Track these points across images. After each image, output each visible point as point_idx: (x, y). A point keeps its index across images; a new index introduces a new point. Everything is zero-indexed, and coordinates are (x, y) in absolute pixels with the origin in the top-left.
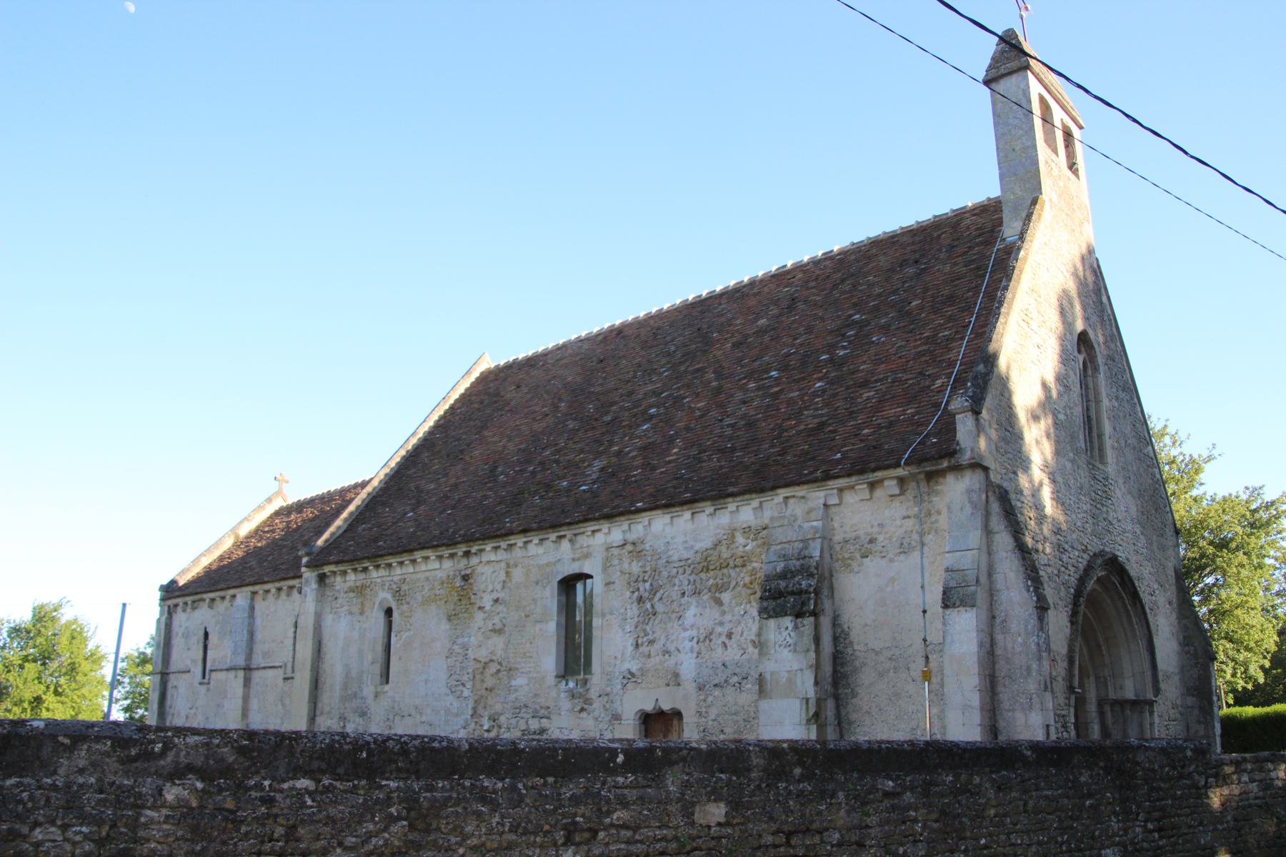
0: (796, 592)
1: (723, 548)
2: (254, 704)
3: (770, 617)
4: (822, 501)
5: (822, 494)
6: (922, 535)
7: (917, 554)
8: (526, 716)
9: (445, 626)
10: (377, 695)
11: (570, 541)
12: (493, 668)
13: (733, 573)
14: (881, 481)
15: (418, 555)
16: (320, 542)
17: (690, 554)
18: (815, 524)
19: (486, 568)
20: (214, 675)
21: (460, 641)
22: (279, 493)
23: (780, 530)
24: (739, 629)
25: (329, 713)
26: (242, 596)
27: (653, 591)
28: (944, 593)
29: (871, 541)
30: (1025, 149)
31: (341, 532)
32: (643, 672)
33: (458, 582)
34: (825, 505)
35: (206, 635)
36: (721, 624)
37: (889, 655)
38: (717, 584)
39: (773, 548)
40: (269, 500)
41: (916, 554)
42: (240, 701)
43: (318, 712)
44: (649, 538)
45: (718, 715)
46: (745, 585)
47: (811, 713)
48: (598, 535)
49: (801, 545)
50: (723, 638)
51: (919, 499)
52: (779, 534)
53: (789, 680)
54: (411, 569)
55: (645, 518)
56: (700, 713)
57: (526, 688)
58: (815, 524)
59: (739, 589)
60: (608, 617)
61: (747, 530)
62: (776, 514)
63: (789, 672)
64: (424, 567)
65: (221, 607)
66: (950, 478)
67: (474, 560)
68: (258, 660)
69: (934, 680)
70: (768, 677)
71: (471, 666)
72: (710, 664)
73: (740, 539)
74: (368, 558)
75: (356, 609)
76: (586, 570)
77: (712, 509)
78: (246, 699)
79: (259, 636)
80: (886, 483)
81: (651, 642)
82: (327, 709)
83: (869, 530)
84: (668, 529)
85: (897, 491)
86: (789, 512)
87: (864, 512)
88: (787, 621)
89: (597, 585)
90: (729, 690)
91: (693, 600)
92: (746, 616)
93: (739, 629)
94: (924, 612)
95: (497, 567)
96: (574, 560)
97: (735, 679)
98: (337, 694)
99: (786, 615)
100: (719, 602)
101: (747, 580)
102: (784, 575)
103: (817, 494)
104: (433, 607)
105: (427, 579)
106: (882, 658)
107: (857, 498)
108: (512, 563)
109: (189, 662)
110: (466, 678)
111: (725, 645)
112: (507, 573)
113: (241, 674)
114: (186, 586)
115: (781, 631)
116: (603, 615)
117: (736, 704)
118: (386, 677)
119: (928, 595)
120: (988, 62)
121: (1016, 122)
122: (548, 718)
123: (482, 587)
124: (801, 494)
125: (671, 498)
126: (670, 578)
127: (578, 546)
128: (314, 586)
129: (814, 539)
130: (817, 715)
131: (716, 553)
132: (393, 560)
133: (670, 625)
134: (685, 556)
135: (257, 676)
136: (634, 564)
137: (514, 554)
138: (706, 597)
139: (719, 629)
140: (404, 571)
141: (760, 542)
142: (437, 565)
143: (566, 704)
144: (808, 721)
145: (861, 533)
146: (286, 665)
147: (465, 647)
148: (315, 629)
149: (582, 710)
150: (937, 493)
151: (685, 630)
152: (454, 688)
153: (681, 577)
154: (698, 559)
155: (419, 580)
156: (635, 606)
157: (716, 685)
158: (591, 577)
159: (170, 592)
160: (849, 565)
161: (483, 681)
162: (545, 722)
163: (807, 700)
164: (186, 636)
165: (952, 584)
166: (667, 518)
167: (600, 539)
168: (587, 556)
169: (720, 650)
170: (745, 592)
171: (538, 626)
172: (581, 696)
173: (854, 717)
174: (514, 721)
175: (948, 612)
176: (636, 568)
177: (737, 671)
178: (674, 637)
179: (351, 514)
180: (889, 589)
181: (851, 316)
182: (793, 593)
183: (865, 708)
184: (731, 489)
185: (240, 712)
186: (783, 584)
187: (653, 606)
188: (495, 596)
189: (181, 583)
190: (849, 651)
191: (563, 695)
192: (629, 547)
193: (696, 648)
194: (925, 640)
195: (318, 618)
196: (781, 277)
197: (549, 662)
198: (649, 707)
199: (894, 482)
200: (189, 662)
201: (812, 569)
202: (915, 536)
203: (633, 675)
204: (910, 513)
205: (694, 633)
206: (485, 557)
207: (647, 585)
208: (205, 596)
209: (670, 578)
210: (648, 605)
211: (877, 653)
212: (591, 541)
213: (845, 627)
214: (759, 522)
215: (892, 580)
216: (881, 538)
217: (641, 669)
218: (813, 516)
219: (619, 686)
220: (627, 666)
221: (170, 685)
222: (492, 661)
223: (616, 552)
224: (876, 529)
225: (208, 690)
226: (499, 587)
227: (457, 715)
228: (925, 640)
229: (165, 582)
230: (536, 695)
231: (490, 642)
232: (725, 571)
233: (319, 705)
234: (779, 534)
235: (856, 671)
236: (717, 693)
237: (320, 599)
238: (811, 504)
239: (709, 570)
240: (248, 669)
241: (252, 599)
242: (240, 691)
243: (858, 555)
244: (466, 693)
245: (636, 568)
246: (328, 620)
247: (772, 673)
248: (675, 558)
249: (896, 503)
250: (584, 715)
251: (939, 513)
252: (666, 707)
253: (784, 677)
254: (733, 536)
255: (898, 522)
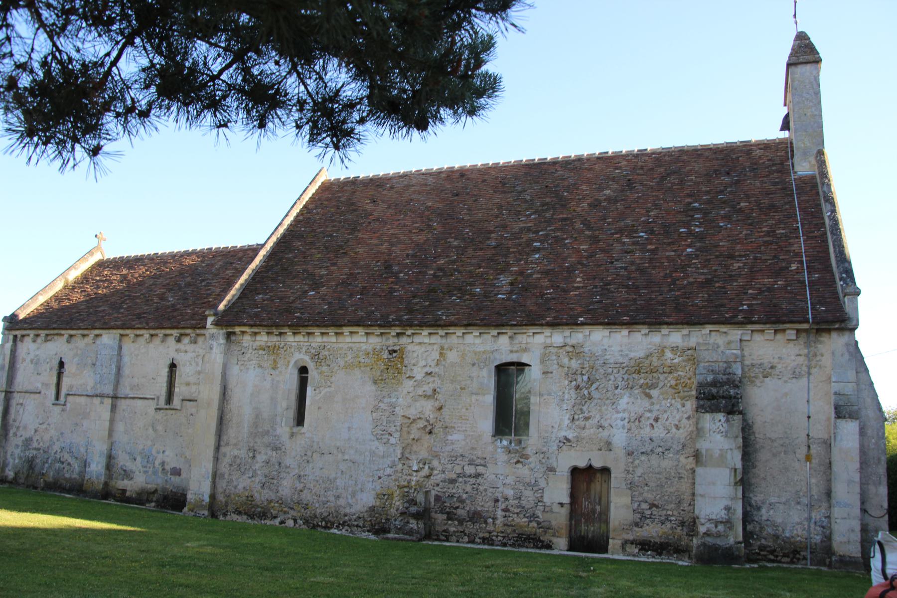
0: (721, 396)
1: (655, 359)
2: (120, 427)
3: (707, 412)
4: (739, 337)
5: (740, 332)
6: (809, 367)
7: (805, 379)
8: (462, 463)
9: (370, 388)
10: (292, 435)
11: (511, 338)
12: (421, 424)
13: (662, 377)
14: (784, 330)
15: (346, 330)
16: (221, 307)
17: (626, 360)
18: (735, 351)
19: (417, 348)
20: (70, 398)
21: (386, 400)
22: (98, 248)
23: (706, 352)
24: (665, 416)
25: (235, 445)
26: (108, 338)
27: (591, 381)
28: (836, 408)
29: (772, 368)
30: (814, 116)
31: (236, 297)
32: (578, 439)
33: (385, 355)
34: (741, 340)
35: (61, 364)
36: (650, 411)
37: (781, 442)
38: (647, 383)
39: (702, 365)
40: (91, 253)
41: (804, 380)
42: (107, 424)
43: (222, 443)
44: (587, 344)
45: (644, 474)
46: (671, 386)
47: (739, 478)
48: (537, 336)
49: (725, 365)
50: (651, 421)
51: (808, 345)
52: (706, 355)
53: (721, 456)
54: (334, 339)
55: (586, 330)
56: (628, 472)
57: (463, 443)
58: (735, 351)
59: (665, 388)
60: (545, 397)
61: (674, 349)
62: (701, 341)
63: (720, 450)
64: (348, 339)
65: (80, 343)
66: (834, 335)
67: (404, 340)
68: (124, 390)
69: (813, 461)
70: (704, 452)
71: (399, 421)
72: (639, 439)
73: (669, 354)
74: (289, 326)
75: (267, 364)
76: (524, 360)
77: (647, 331)
78: (112, 421)
79: (126, 371)
80: (788, 332)
81: (587, 419)
82: (233, 441)
83: (772, 361)
84: (606, 341)
85: (794, 338)
86: (712, 341)
87: (767, 348)
88: (721, 416)
89: (534, 373)
90: (654, 457)
91: (627, 392)
92: (672, 408)
93: (665, 416)
94: (809, 417)
95: (429, 348)
96: (512, 352)
97: (660, 449)
98: (246, 430)
99: (720, 412)
100: (649, 396)
101: (673, 383)
102: (714, 383)
103: (736, 332)
104: (357, 371)
105: (350, 348)
106: (776, 444)
107: (762, 338)
108: (446, 346)
109: (39, 385)
110: (393, 429)
111: (652, 425)
112: (441, 354)
113: (108, 401)
114: (25, 319)
115: (715, 424)
116: (541, 395)
117: (659, 466)
118: (300, 420)
119: (811, 407)
120: (789, 51)
121: (808, 96)
122: (485, 466)
123: (413, 362)
124: (725, 330)
125: (610, 319)
126: (606, 375)
127: (516, 341)
128: (222, 341)
129: (735, 362)
130: (742, 480)
131: (648, 362)
132: (317, 331)
133: (604, 408)
134: (621, 360)
135: (122, 404)
136: (573, 361)
137: (449, 340)
138: (637, 391)
139: (648, 415)
140: (325, 339)
141: (685, 358)
142: (364, 339)
143: (502, 457)
144: (736, 484)
145: (765, 361)
146: (158, 398)
147: (393, 406)
148: (11, 351)
149: (518, 462)
150: (821, 342)
151: (618, 412)
152: (382, 435)
153: (616, 375)
154: (632, 364)
155: (341, 348)
156: (573, 392)
157: (643, 453)
158: (530, 366)
159: (12, 322)
160: (753, 382)
161: (409, 433)
162: (481, 469)
163: (735, 470)
164: (36, 362)
165: (841, 403)
166: (606, 332)
167: (539, 339)
168: (525, 350)
169: (648, 429)
170: (671, 391)
171: (474, 398)
172: (517, 452)
173: (753, 481)
174: (450, 466)
175: (839, 421)
176: (575, 364)
177: (662, 444)
178: (608, 416)
179: (242, 285)
180: (783, 400)
181: (691, 203)
182: (723, 397)
183: (762, 475)
184: (666, 320)
185: (107, 433)
186: (714, 390)
187: (589, 394)
188: (428, 370)
189: (21, 317)
190: (752, 438)
191: (499, 450)
192: (569, 349)
193: (627, 426)
194: (808, 435)
195: (225, 366)
196: (604, 160)
197: (486, 423)
198: (582, 464)
199: (795, 332)
200: (39, 385)
201: (737, 383)
202: (805, 368)
203: (568, 440)
204: (801, 352)
205: (626, 415)
206: (417, 339)
207: (585, 378)
208: (63, 332)
209: (606, 375)
210: (586, 392)
211: (773, 441)
212: (530, 340)
213: (750, 422)
214: (685, 344)
215: (786, 394)
216: (779, 366)
217: (577, 437)
218: (733, 346)
219: (555, 448)
220: (563, 434)
221: (13, 403)
222: (420, 418)
223: (554, 350)
224: (776, 360)
225: (63, 410)
226: (433, 364)
227: (383, 457)
228: (808, 435)
229: (8, 315)
230: (473, 448)
231: (418, 404)
232: (654, 375)
233: (224, 438)
234: (706, 355)
235: (756, 451)
236: (643, 458)
237: (227, 352)
238: (730, 338)
239: (642, 374)
240: (115, 397)
241: (120, 340)
242: (107, 415)
243: (761, 375)
244: (393, 440)
245: (575, 364)
246: (235, 370)
247: (707, 450)
248: (612, 361)
249: (791, 345)
250: (520, 465)
251: (822, 355)
252: (597, 464)
253: (717, 453)
254: (663, 351)
255: (793, 358)
